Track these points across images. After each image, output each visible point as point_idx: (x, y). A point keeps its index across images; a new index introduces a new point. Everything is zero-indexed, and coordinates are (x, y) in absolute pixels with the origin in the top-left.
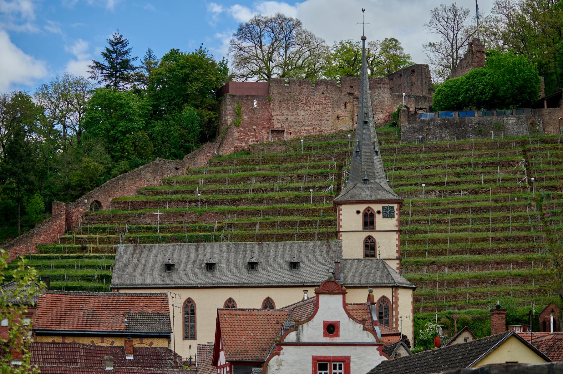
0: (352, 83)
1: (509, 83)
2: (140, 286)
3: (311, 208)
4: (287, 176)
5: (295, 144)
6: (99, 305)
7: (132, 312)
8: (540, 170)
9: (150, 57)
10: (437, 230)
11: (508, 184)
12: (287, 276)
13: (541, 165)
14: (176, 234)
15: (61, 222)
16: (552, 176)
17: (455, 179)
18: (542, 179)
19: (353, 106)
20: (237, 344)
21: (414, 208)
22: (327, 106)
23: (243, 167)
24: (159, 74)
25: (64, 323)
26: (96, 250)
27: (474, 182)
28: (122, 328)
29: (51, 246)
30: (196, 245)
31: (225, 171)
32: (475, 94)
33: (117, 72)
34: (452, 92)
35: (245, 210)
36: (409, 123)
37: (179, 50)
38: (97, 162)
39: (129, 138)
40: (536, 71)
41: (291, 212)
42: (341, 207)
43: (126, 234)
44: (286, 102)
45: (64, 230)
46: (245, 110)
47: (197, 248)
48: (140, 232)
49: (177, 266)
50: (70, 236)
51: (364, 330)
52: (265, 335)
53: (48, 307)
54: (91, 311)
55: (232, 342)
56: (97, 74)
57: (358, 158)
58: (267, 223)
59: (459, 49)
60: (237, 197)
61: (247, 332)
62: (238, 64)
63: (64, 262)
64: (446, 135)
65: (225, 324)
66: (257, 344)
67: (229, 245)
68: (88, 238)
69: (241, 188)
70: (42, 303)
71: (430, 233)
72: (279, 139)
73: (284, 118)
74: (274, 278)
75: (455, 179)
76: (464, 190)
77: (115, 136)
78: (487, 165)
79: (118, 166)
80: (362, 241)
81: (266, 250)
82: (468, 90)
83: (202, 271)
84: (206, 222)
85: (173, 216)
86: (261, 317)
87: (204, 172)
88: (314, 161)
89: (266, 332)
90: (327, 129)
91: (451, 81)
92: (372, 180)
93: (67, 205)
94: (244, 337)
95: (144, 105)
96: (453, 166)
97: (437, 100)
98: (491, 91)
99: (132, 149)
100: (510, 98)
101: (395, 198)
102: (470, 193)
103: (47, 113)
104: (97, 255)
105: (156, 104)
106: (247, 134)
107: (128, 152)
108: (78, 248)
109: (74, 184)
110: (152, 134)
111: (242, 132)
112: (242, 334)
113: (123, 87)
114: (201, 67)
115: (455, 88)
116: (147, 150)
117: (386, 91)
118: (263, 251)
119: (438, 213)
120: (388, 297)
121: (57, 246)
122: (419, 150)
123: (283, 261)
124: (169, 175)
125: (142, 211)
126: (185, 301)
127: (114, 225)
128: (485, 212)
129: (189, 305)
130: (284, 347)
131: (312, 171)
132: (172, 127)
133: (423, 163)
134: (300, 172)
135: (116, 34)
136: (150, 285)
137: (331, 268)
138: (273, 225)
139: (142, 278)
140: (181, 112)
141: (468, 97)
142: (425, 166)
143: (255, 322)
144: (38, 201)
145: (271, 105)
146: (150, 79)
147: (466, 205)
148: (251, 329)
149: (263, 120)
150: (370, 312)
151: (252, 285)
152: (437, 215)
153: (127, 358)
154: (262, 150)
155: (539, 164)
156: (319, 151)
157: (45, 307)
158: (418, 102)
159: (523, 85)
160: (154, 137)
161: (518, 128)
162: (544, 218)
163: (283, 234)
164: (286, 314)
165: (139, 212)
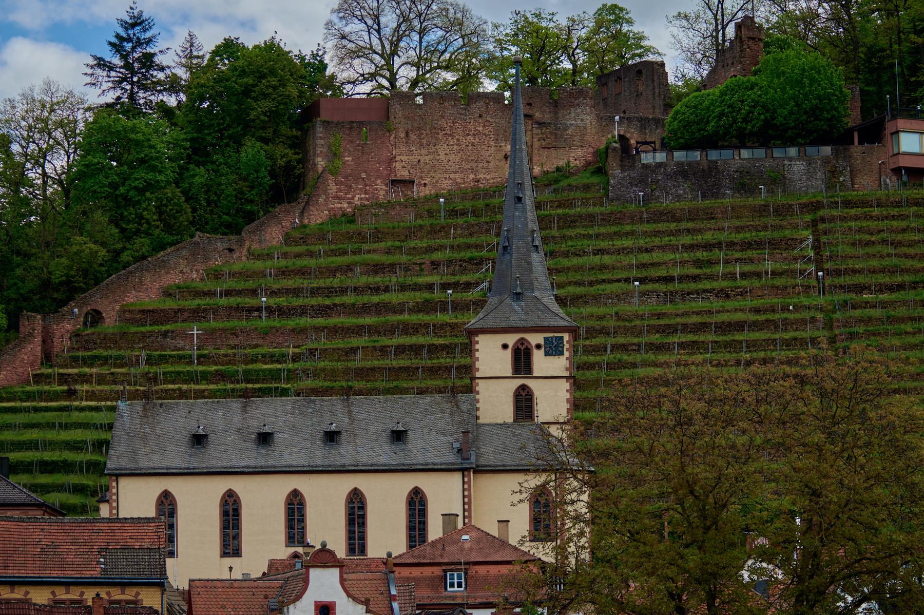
0: (531, 98)
1: (792, 103)
3: (448, 321)
4: (414, 264)
5: (427, 207)
7: (110, 547)
9: (192, 45)
10: (654, 362)
11: (780, 282)
12: (385, 454)
13: (839, 248)
14: (223, 368)
15: (34, 347)
16: (857, 267)
18: (838, 273)
19: (533, 138)
21: (621, 323)
22: (488, 138)
26: (91, 396)
27: (726, 277)
28: (95, 572)
29: (16, 389)
30: (243, 402)
31: (311, 254)
32: (735, 121)
33: (134, 73)
34: (697, 116)
35: (340, 325)
36: (623, 171)
37: (238, 38)
38: (95, 242)
39: (150, 200)
41: (415, 329)
42: (477, 339)
45: (39, 361)
47: (245, 407)
49: (212, 437)
50: (50, 371)
51: (367, 612)
56: (100, 78)
57: (507, 257)
58: (374, 347)
60: (328, 302)
64: (684, 190)
65: (197, 599)
67: (295, 403)
68: (80, 375)
69: (335, 286)
71: (642, 367)
72: (405, 195)
73: (414, 159)
74: (365, 458)
78: (747, 245)
79: (131, 247)
81: (355, 409)
82: (722, 114)
84: (274, 345)
85: (220, 336)
87: (276, 257)
91: (696, 97)
92: (528, 294)
93: (44, 319)
95: (176, 140)
97: (673, 130)
99: (155, 217)
100: (794, 128)
101: (566, 324)
102: (716, 296)
105: (198, 138)
108: (63, 392)
109: (57, 281)
110: (190, 190)
111: (342, 183)
114: (273, 72)
115: (703, 110)
118: (350, 412)
119: (658, 332)
121: (28, 388)
122: (638, 217)
123: (380, 427)
124: (217, 262)
125: (168, 327)
127: (123, 351)
128: (738, 331)
129: (231, 501)
131: (456, 255)
132: (223, 178)
133: (641, 242)
134: (437, 256)
135: (131, 8)
137: (458, 441)
138: (384, 351)
139: (155, 458)
140: (238, 152)
141: (723, 126)
145: (392, 138)
147: (706, 319)
148: (232, 607)
150: (388, 583)
151: (330, 469)
152: (658, 335)
154: (376, 215)
155: (837, 246)
156: (471, 219)
158: (645, 129)
160: (193, 194)
161: (808, 179)
162: (835, 342)
163: (400, 368)
165: (164, 328)
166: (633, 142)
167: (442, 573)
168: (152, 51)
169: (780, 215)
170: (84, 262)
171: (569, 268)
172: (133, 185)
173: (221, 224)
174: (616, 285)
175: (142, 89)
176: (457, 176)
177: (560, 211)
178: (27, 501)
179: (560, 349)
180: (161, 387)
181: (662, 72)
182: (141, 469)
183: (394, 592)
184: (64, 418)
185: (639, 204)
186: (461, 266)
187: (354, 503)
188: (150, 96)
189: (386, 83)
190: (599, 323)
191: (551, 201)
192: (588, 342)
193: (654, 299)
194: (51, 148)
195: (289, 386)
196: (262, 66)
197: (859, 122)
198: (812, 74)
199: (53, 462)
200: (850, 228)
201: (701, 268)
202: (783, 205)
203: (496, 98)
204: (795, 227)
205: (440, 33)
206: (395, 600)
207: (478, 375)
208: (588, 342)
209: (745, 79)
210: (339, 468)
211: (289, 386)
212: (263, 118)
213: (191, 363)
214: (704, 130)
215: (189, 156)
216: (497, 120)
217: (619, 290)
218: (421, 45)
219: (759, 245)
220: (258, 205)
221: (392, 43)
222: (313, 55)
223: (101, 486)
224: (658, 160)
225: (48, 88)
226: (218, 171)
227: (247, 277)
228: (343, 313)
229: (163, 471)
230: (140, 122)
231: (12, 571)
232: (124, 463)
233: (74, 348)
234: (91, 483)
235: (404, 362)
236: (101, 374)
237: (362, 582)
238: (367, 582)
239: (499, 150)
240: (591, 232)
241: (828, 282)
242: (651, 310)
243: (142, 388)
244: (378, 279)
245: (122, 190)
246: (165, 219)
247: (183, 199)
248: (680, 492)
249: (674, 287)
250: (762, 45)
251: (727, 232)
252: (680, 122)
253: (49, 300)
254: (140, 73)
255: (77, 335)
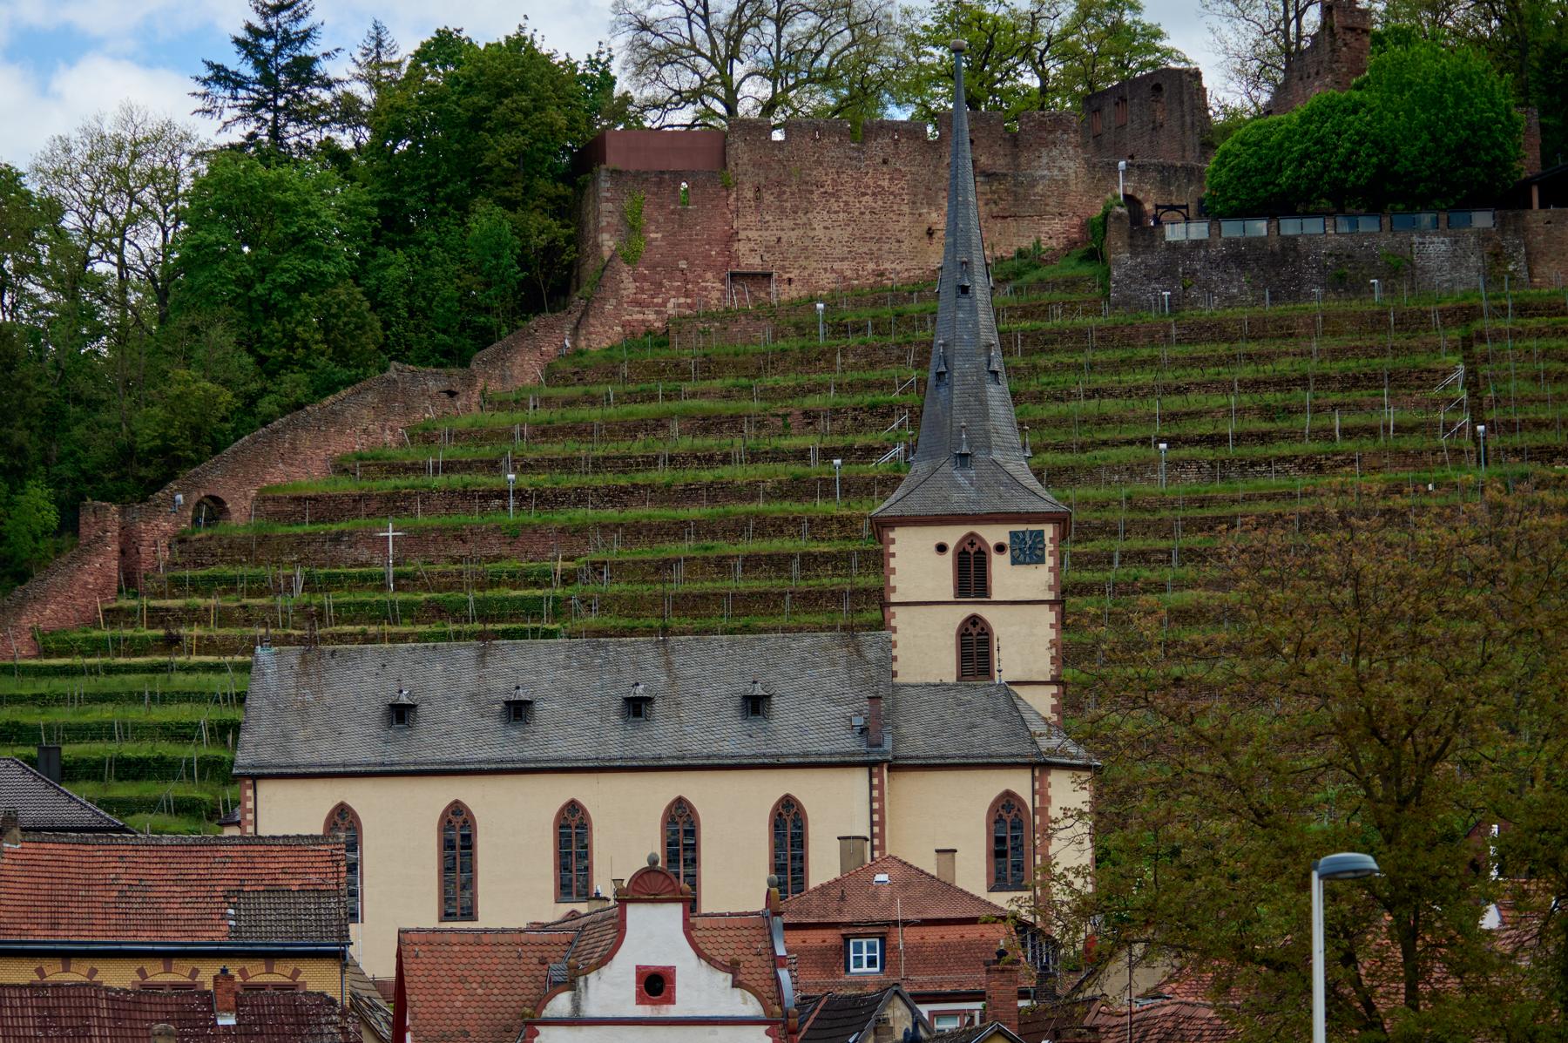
1: (1425, 136)
2: (317, 770)
3: (835, 513)
4: (773, 415)
5: (797, 318)
6: (162, 872)
7: (246, 889)
8: (1509, 399)
9: (379, 44)
11: (1411, 443)
12: (733, 737)
13: (1512, 386)
15: (107, 561)
16: (1543, 416)
17: (1257, 425)
18: (1510, 427)
20: (443, 1016)
21: (1137, 516)
23: (645, 386)
24: (397, 109)
25: (66, 921)
26: (207, 646)
28: (218, 934)
31: (592, 400)
32: (1326, 168)
33: (278, 93)
34: (1260, 159)
35: (645, 521)
36: (1134, 254)
38: (213, 380)
39: (308, 306)
40: (1507, 98)
41: (778, 527)
42: (892, 535)
43: (299, 596)
44: (776, 190)
45: (115, 586)
46: (656, 214)
47: (483, 656)
48: (337, 588)
49: (424, 710)
52: (512, 992)
53: (27, 880)
54: (139, 888)
55: (432, 1010)
56: (220, 102)
57: (943, 391)
58: (706, 559)
59: (1304, 10)
60: (623, 481)
61: (467, 985)
62: (641, 68)
63: (113, 683)
64: (1240, 288)
65: (414, 966)
66: (491, 1016)
68: (186, 610)
69: (636, 454)
70: (9, 867)
72: (756, 299)
73: (770, 236)
74: (696, 744)
75: (1257, 425)
76: (1281, 459)
77: (267, 300)
78: (1353, 382)
79: (276, 388)
80: (953, 632)
81: (677, 660)
82: (1306, 155)
83: (493, 723)
84: (530, 556)
85: (435, 540)
86: (502, 949)
87: (532, 405)
88: (854, 367)
89: (516, 985)
90: (898, 268)
91: (1259, 127)
93: (122, 513)
94: (461, 998)
95: (354, 203)
96: (1255, 385)
97: (1219, 184)
98: (1374, 160)
99: (318, 337)
101: (1047, 508)
103: (70, 221)
104: (210, 659)
105: (392, 200)
106: (661, 285)
107: (305, 346)
108: (156, 639)
109: (146, 447)
110: (379, 290)
111: (644, 278)
112: (456, 991)
113: (296, 139)
114: (522, 88)
115: (1270, 148)
116: (363, 339)
117: (1071, 152)
118: (669, 663)
119: (1201, 530)
120: (1019, 793)
121: (95, 633)
122: (1162, 333)
123: (723, 691)
124: (428, 413)
125: (343, 526)
126: (446, 811)
130: (542, 1029)
131: (847, 401)
132: (437, 268)
133: (1168, 377)
134: (812, 402)
136: (344, 766)
138: (722, 565)
141: (1307, 176)
142: (1174, 386)
143: (488, 961)
144: (38, 502)
145: (731, 199)
146: (373, 119)
147: (1283, 507)
149: (709, 244)
150: (771, 934)
151: (635, 763)
152: (1199, 537)
153: (220, 1022)
154: (705, 333)
155: (1506, 380)
156: (870, 337)
157: (18, 880)
158: (1169, 185)
159: (1466, 140)
160: (384, 298)
161: (1453, 268)
163: (752, 594)
164: (565, 941)
165: (335, 528)
166: (1148, 207)
167: (840, 942)
168: (310, 54)
169: (1407, 330)
170: (194, 414)
171: (1043, 421)
172: (279, 280)
173: (434, 351)
174: (1127, 450)
175: (293, 120)
176: (845, 265)
177: (1026, 324)
178: (94, 824)
179: (1038, 552)
180: (330, 629)
181: (1196, 87)
182: (297, 767)
183: (781, 951)
184: (159, 683)
185: (1163, 311)
186: (856, 419)
187: (677, 823)
188: (307, 131)
189: (720, 108)
190: (1098, 514)
191: (1010, 308)
192: (1079, 548)
193: (1192, 474)
194: (132, 219)
195: (556, 626)
196: (503, 75)
197: (1538, 170)
198: (1459, 86)
199: (140, 761)
200: (1529, 351)
201: (1272, 420)
202: (1412, 313)
203: (911, 131)
204: (1435, 350)
205: (813, 20)
206: (783, 966)
207: (894, 598)
208: (1079, 548)
209: (1343, 95)
210: (650, 763)
211: (556, 626)
212: (506, 163)
213: (383, 588)
214: (1273, 183)
215: (376, 232)
216: (913, 169)
217: (1132, 459)
218: (779, 41)
219: (1372, 380)
220: (498, 316)
221: (728, 38)
222: (590, 61)
223: (225, 802)
224: (1193, 236)
225: (128, 116)
226: (428, 256)
227: (481, 439)
228: (651, 500)
229: (337, 770)
230: (289, 173)
231: (67, 933)
232: (267, 755)
233: (176, 564)
234: (207, 797)
235: (758, 585)
236: (224, 608)
237: (723, 933)
238: (731, 933)
239: (917, 221)
240: (1080, 360)
241: (1494, 441)
242: (1188, 493)
243: (296, 632)
244: (711, 441)
245: (260, 289)
246: (335, 340)
247: (367, 304)
248: (1353, 733)
249: (1227, 452)
250: (1368, 40)
251: (1316, 359)
252: (1231, 170)
253: (131, 480)
254: (289, 92)
255: (182, 541)
